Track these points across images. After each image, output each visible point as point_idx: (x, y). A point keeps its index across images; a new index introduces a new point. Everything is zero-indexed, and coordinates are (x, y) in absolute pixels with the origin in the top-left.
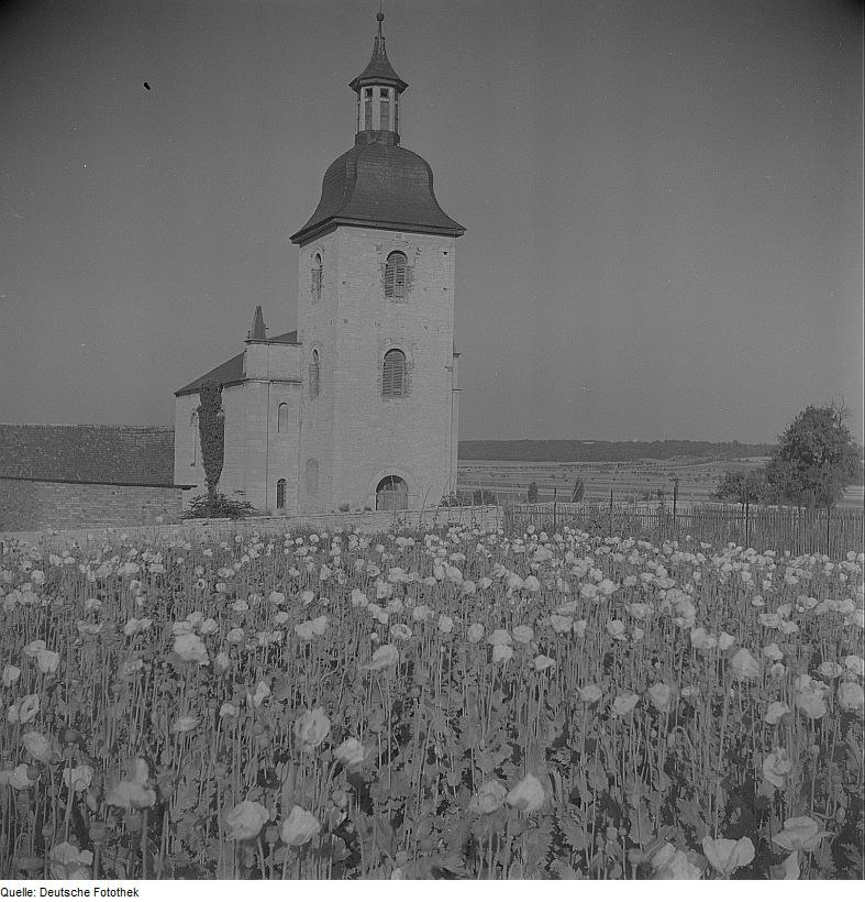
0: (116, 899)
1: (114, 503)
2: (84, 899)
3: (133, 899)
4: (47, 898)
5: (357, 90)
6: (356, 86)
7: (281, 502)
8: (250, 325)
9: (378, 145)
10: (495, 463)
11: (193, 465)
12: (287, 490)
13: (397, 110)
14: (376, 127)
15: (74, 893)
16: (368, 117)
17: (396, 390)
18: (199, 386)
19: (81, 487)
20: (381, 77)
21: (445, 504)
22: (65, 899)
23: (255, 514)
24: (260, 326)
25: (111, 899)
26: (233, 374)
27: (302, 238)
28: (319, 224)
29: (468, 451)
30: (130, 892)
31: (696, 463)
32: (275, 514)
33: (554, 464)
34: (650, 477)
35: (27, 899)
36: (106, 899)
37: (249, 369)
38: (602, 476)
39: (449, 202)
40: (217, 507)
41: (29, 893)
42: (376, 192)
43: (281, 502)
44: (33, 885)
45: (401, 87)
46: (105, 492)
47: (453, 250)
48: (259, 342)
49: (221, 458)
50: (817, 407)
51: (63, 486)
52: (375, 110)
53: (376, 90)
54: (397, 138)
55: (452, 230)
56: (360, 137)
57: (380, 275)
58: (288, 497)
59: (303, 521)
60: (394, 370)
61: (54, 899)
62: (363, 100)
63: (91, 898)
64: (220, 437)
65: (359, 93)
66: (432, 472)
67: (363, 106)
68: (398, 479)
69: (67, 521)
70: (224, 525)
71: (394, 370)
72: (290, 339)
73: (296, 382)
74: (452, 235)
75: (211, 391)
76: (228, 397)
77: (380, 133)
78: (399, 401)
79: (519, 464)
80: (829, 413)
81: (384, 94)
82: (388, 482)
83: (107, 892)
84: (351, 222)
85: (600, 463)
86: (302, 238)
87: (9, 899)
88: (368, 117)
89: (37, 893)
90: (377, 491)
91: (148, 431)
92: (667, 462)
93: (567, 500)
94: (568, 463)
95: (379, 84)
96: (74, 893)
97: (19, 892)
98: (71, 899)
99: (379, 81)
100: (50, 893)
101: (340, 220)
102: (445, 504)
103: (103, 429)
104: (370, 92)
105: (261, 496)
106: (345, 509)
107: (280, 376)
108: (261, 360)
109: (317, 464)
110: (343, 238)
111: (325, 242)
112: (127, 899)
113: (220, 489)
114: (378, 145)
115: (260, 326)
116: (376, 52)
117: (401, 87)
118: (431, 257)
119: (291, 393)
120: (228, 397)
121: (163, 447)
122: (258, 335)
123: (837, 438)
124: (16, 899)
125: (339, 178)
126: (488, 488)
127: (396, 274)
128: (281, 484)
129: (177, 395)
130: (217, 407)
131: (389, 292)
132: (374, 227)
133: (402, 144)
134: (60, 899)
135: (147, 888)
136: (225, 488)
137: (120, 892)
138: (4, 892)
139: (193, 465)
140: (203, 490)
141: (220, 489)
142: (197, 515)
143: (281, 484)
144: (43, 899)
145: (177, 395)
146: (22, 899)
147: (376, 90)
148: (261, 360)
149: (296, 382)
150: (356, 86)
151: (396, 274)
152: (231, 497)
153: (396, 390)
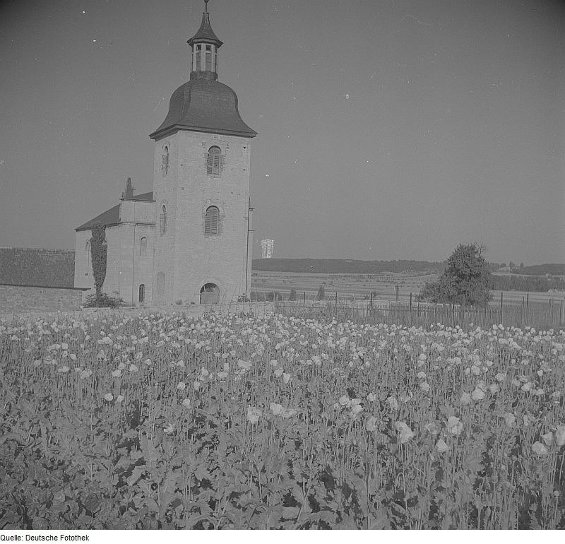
0: (75, 542)
1: (41, 298)
2: (54, 542)
3: (86, 542)
4: (31, 542)
5: (192, 45)
6: (191, 42)
7: (141, 298)
8: (124, 189)
9: (203, 80)
10: (288, 274)
11: (86, 275)
12: (145, 291)
13: (216, 58)
14: (203, 69)
15: (48, 538)
16: (198, 62)
17: (213, 231)
18: (91, 226)
19: (22, 288)
20: (206, 38)
21: (239, 301)
22: (42, 542)
23: (125, 306)
24: (130, 189)
25: (71, 542)
26: (111, 219)
27: (157, 136)
28: (167, 128)
29: (260, 265)
30: (83, 537)
31: (419, 275)
32: (138, 306)
33: (325, 275)
34: (388, 284)
35: (17, 542)
36: (68, 542)
37: (123, 216)
38: (358, 283)
39: (248, 115)
40: (102, 301)
41: (18, 538)
42: (201, 108)
43: (141, 298)
44: (22, 533)
45: (218, 44)
46: (35, 291)
47: (249, 146)
48: (130, 200)
49: (105, 270)
50: (465, 245)
51: (11, 288)
52: (203, 59)
53: (203, 46)
54: (216, 76)
55: (247, 133)
56: (193, 75)
57: (204, 161)
58: (145, 295)
59: (155, 310)
60: (212, 220)
61: (35, 542)
62: (195, 52)
63: (59, 541)
64: (104, 257)
65: (193, 47)
66: (235, 281)
67: (195, 55)
68: (214, 286)
69: (12, 309)
70: (108, 311)
71: (212, 220)
72: (148, 197)
73: (152, 225)
74: (249, 137)
75: (100, 227)
76: (109, 233)
77: (206, 72)
78: (214, 237)
79: (303, 275)
80: (473, 248)
81: (208, 48)
82: (209, 286)
83: (69, 538)
84: (187, 128)
85: (356, 275)
86: (157, 136)
87: (6, 542)
88: (198, 62)
89: (24, 538)
90: (201, 292)
91: (57, 252)
92: (400, 274)
93: (312, 298)
94: (335, 274)
95: (205, 42)
96: (48, 538)
97: (12, 537)
98: (45, 542)
99: (205, 40)
100: (32, 538)
101: (177, 126)
102: (239, 301)
103: (29, 251)
104: (199, 47)
105: (129, 294)
106: (180, 303)
107: (142, 221)
108: (130, 211)
109: (164, 275)
110: (182, 139)
111: (171, 139)
112: (82, 542)
113: (104, 290)
114: (203, 80)
115: (130, 189)
116: (203, 22)
117: (218, 44)
118: (236, 151)
119: (149, 230)
120: (109, 233)
121: (68, 263)
122: (129, 195)
123: (477, 263)
124: (10, 542)
125: (180, 99)
126: (277, 290)
127: (214, 161)
128: (142, 287)
129: (77, 230)
130: (102, 239)
131: (209, 171)
132: (200, 131)
133: (219, 80)
134: (39, 542)
135: (96, 535)
136: (107, 290)
137: (77, 537)
138: (3, 537)
139: (86, 275)
140: (94, 291)
141: (104, 290)
142: (90, 306)
143: (142, 287)
144: (27, 542)
145: (77, 230)
146: (14, 542)
147: (203, 46)
148: (130, 211)
149: (152, 225)
150: (191, 42)
151: (214, 161)
152: (111, 295)
153: (213, 231)
